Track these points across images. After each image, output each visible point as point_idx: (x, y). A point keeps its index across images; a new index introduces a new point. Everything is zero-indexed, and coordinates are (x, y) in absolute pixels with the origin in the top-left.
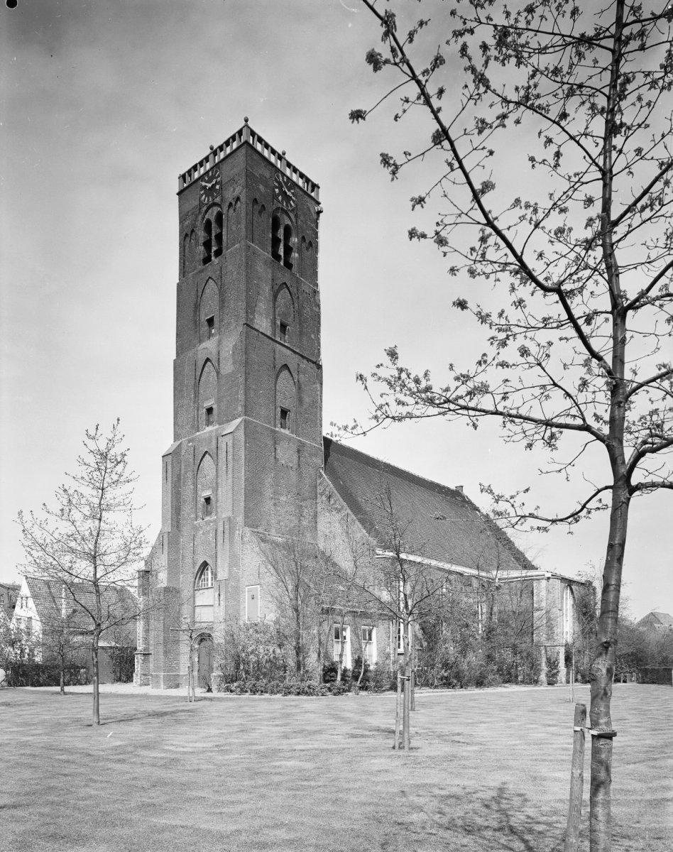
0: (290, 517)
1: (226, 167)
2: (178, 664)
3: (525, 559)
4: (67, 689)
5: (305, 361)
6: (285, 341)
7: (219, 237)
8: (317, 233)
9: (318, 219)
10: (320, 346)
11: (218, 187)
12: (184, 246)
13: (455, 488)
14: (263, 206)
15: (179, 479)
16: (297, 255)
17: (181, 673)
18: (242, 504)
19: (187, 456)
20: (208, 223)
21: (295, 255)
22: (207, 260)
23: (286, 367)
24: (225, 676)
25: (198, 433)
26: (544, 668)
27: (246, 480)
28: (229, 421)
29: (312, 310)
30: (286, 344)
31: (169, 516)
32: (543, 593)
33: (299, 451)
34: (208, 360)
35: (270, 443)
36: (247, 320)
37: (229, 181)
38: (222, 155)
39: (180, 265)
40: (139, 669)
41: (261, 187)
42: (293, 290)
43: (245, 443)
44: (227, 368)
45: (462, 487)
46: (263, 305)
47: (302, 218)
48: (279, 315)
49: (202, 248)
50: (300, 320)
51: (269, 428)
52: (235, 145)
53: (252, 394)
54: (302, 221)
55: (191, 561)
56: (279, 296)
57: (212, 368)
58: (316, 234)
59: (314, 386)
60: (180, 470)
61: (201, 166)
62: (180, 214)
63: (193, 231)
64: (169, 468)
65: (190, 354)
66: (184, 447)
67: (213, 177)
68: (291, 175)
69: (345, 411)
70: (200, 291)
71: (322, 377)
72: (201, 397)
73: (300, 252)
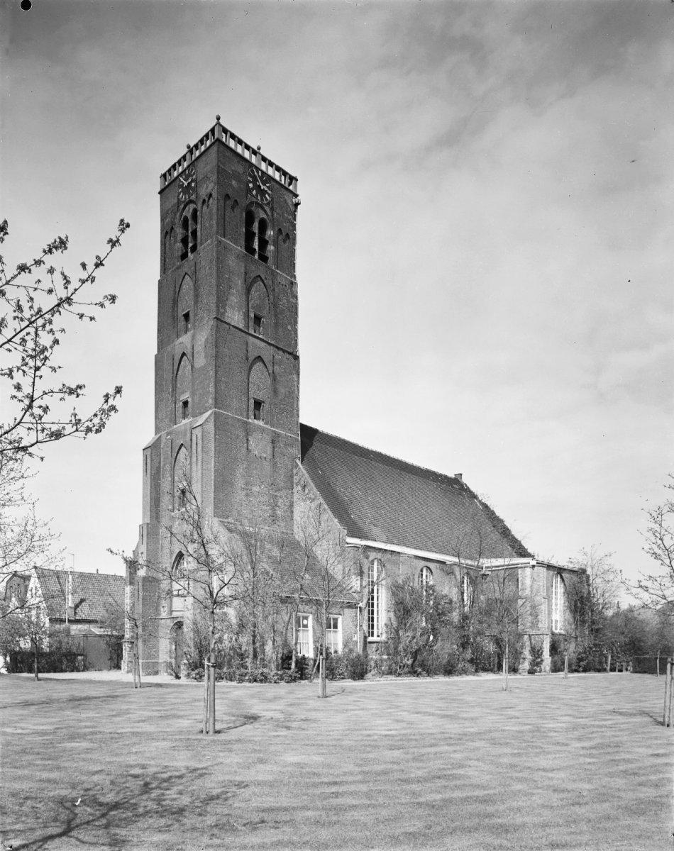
0: (265, 508)
1: (200, 164)
2: (157, 652)
3: (521, 546)
4: (40, 675)
5: (281, 353)
6: (260, 334)
7: (194, 233)
8: (295, 225)
9: (295, 211)
10: (297, 337)
11: (193, 185)
12: (165, 244)
13: (454, 476)
14: (236, 201)
15: (158, 472)
16: (272, 248)
17: (160, 661)
18: (212, 495)
19: (165, 448)
20: (186, 220)
21: (271, 248)
22: (184, 256)
23: (259, 358)
24: (189, 664)
25: (175, 426)
26: (527, 653)
27: (215, 471)
28: (201, 414)
29: (288, 301)
30: (261, 336)
31: (149, 508)
32: (528, 582)
33: (273, 442)
34: (184, 354)
35: (242, 434)
36: (218, 314)
37: (203, 178)
38: (197, 153)
39: (161, 263)
40: (127, 656)
41: (234, 182)
42: (269, 282)
43: (215, 435)
44: (200, 361)
45: (461, 474)
46: (235, 298)
47: (278, 211)
48: (253, 308)
49: (180, 245)
50: (276, 311)
51: (240, 420)
52: (208, 143)
53: (223, 386)
54: (278, 214)
55: (168, 551)
56: (253, 289)
57: (187, 363)
58: (294, 226)
59: (290, 377)
60: (160, 463)
61: (180, 165)
62: (161, 212)
63: (172, 228)
64: (149, 461)
65: (169, 348)
66: (163, 440)
67: (190, 175)
68: (267, 169)
69: (331, 398)
70: (178, 286)
71: (299, 368)
72: (178, 391)
73: (276, 244)
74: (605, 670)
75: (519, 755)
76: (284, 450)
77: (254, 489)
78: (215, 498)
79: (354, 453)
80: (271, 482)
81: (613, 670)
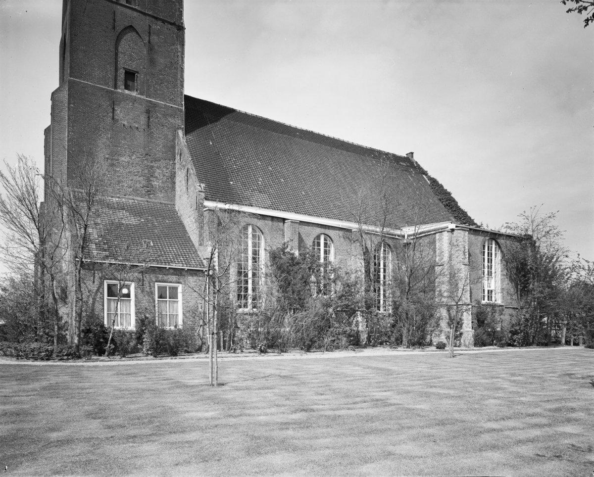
0: (137, 178)
5: (160, 23)
10: (182, 8)
13: (406, 156)
23: (131, 28)
33: (148, 112)
43: (69, 104)
74: (557, 343)
75: (575, 365)
76: (163, 121)
77: (123, 159)
78: (68, 168)
79: (274, 130)
80: (144, 153)
81: (568, 343)
